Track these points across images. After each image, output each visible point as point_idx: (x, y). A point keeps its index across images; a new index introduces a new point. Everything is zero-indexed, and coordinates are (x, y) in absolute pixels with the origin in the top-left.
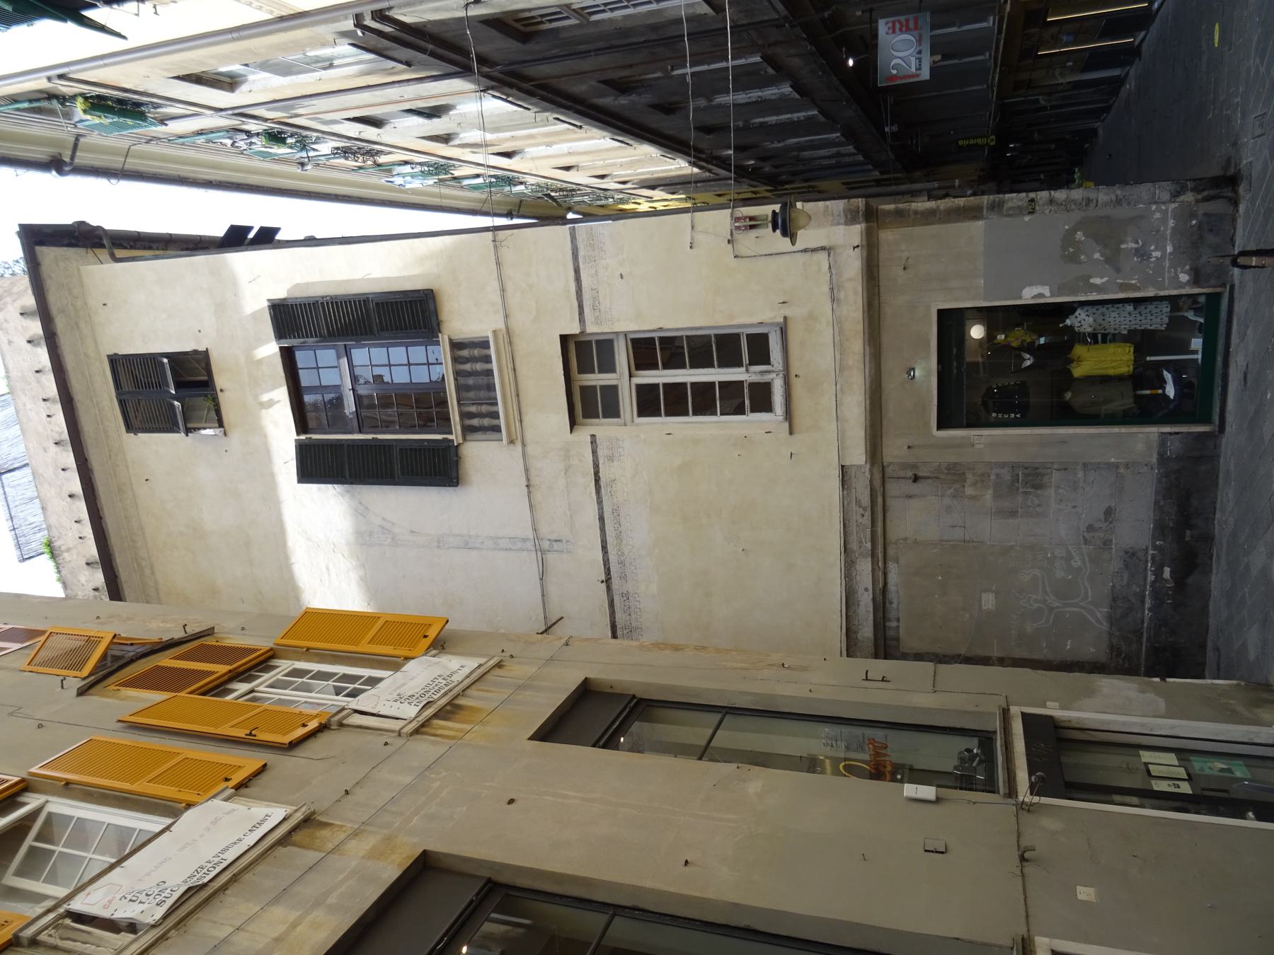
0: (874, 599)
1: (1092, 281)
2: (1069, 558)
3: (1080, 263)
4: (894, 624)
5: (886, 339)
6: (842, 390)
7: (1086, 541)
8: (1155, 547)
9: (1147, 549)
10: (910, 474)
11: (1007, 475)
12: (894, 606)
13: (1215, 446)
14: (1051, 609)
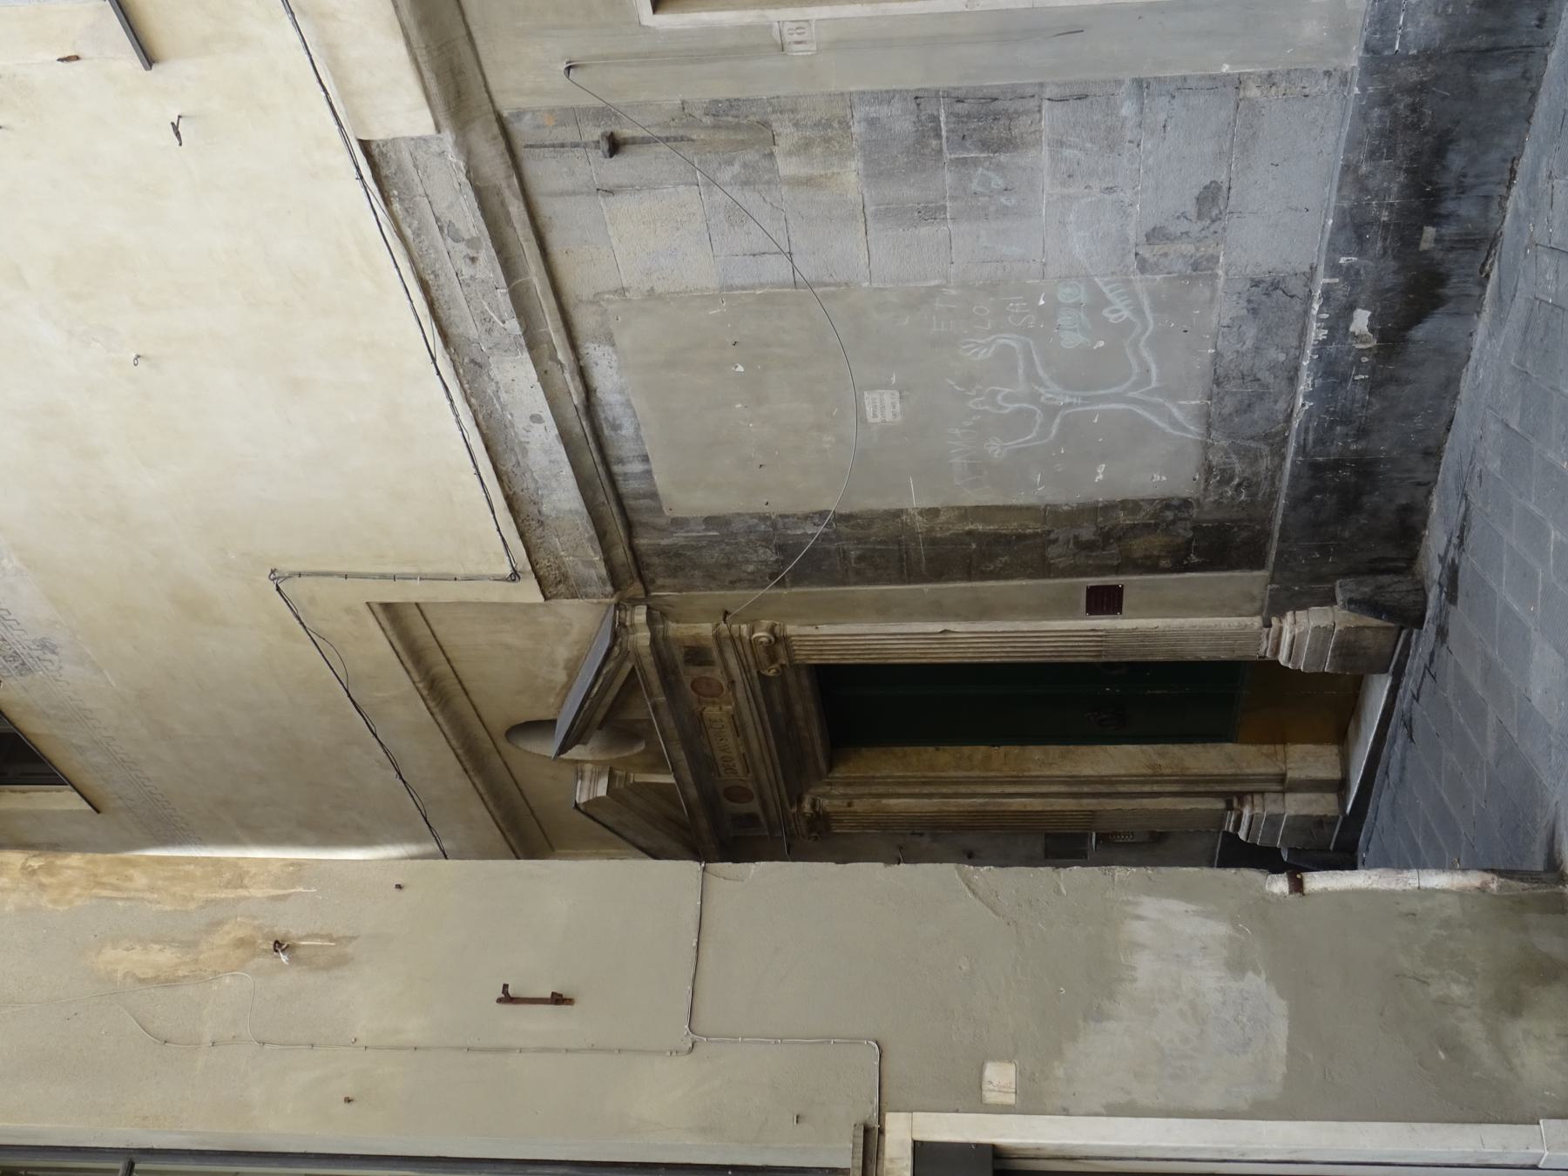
0: (565, 437)
2: (1098, 302)
4: (637, 467)
7: (1143, 266)
8: (1334, 269)
9: (1313, 269)
10: (594, 133)
11: (902, 123)
12: (627, 430)
13: (1541, 20)
14: (1051, 411)
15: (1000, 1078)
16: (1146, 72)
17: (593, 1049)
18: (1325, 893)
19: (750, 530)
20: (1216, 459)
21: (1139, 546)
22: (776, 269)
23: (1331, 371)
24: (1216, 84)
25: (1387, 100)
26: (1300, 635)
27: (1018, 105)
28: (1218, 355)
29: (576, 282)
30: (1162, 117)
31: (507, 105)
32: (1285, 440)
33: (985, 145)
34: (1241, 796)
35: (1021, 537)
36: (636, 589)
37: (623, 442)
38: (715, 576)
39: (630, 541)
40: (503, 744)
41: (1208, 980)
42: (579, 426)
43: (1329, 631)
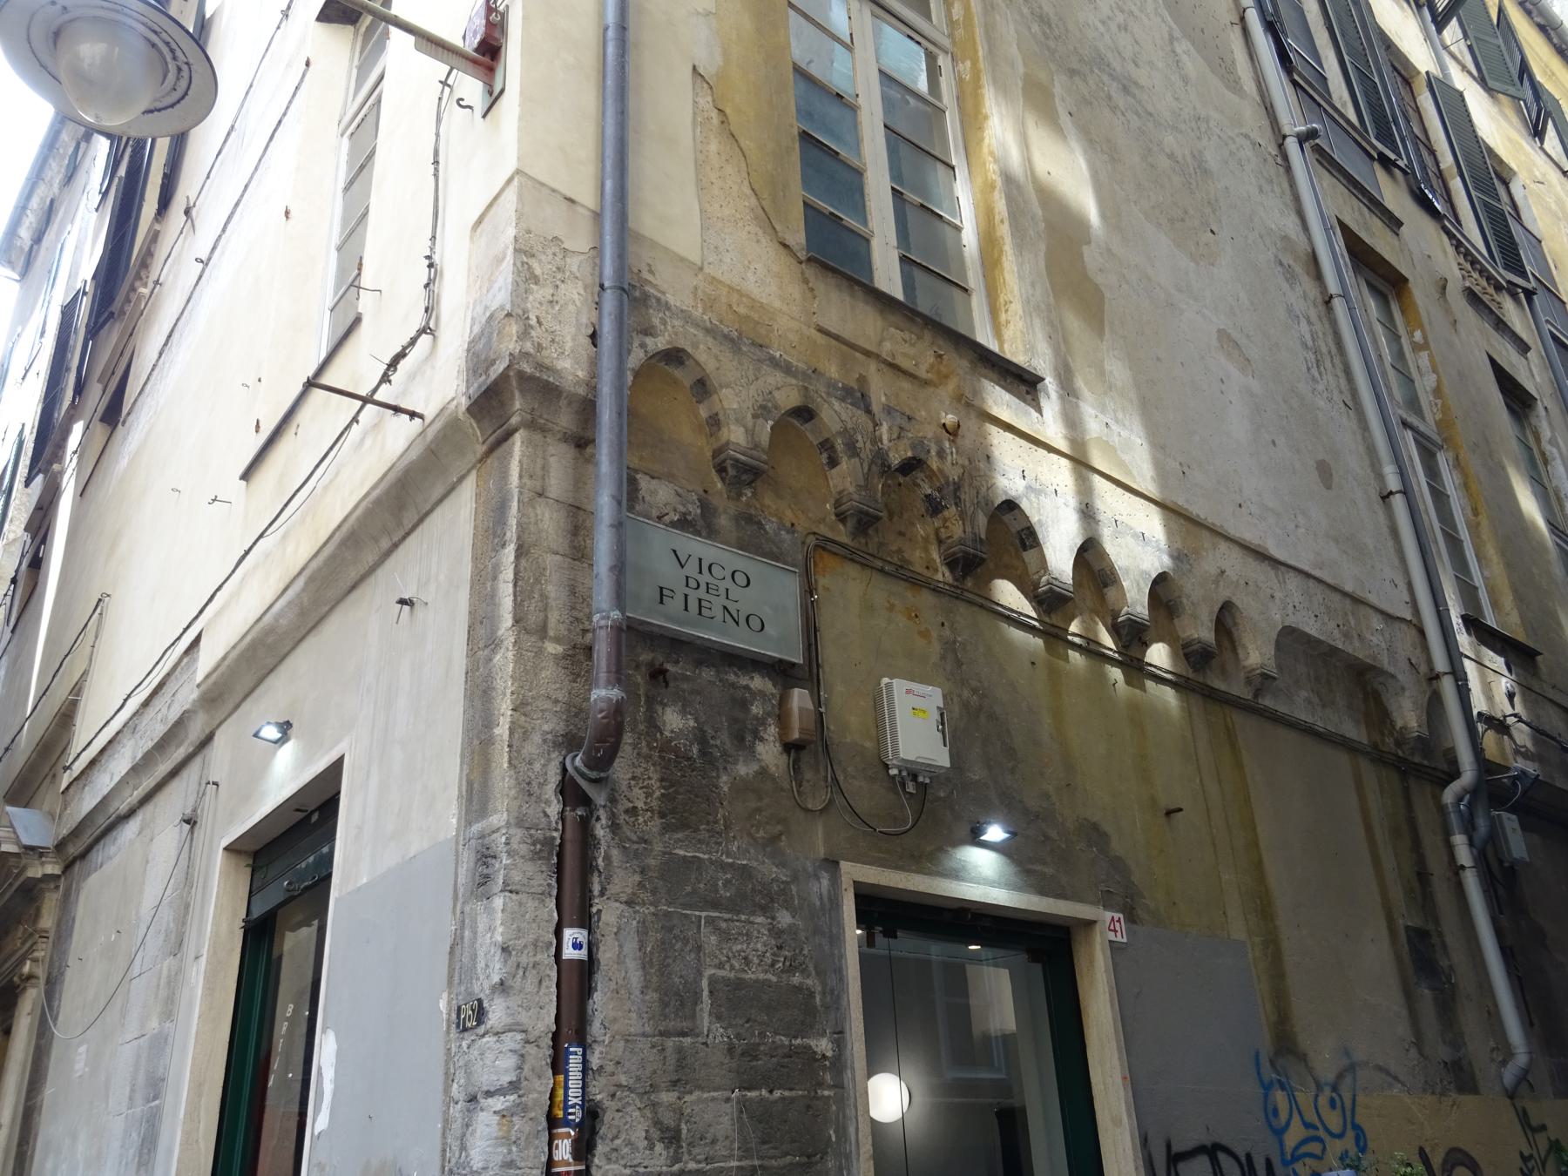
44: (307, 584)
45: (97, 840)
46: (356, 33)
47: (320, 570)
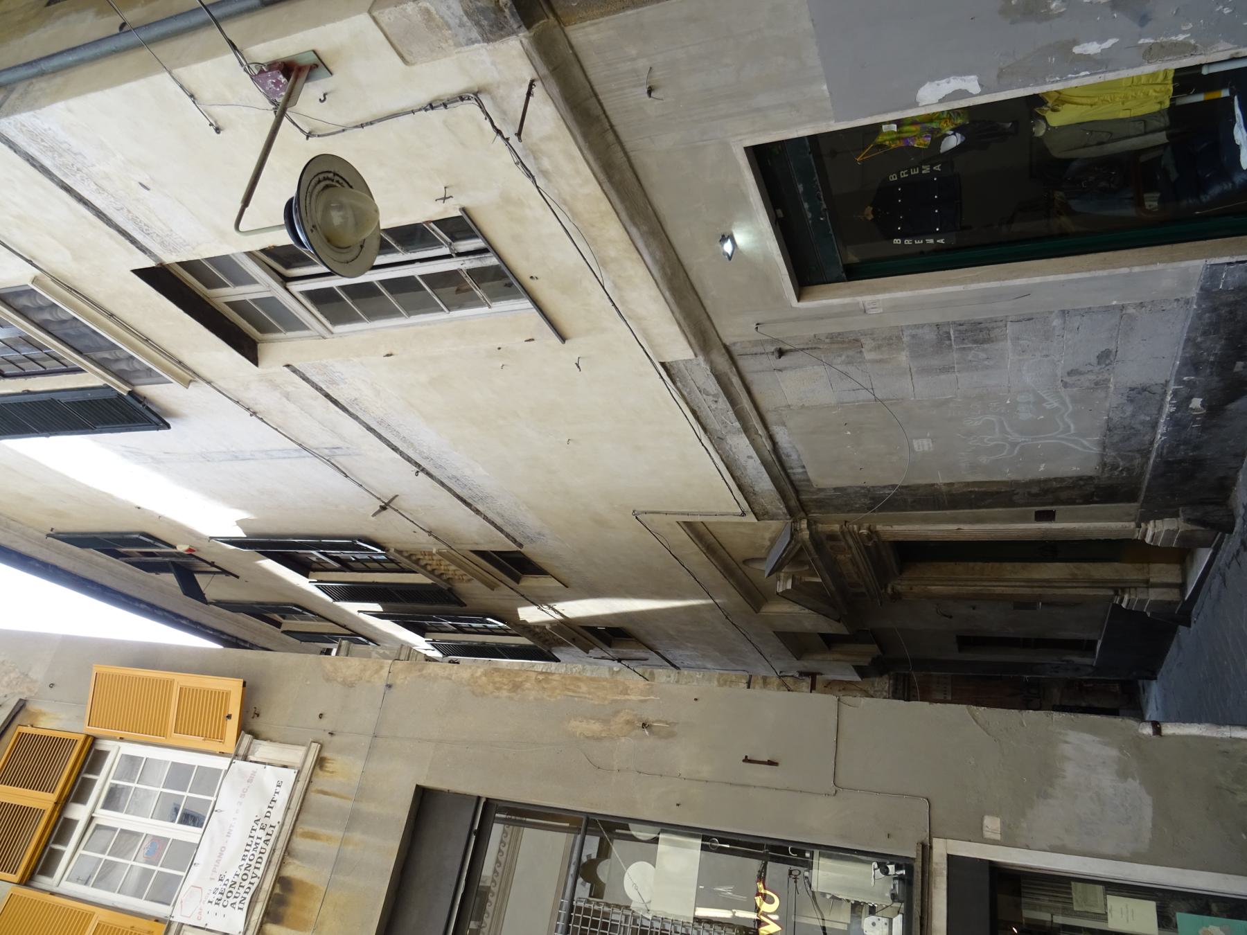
1: (1077, 50)
3: (1048, 16)
4: (800, 470)
5: (663, 201)
6: (616, 286)
7: (1065, 385)
8: (1179, 381)
9: (1167, 382)
11: (931, 336)
12: (794, 457)
14: (1014, 445)
15: (992, 825)
16: (1067, 307)
17: (788, 790)
18: (1174, 736)
19: (856, 492)
20: (1108, 460)
21: (1064, 495)
22: (864, 395)
23: (1176, 422)
24: (1108, 309)
25: (1214, 310)
26: (1156, 530)
27: (994, 325)
28: (1110, 419)
29: (764, 403)
30: (1076, 325)
31: (727, 341)
32: (1150, 452)
33: (975, 342)
34: (1123, 590)
35: (998, 493)
36: (802, 514)
37: (793, 460)
38: (838, 509)
39: (794, 492)
40: (742, 566)
41: (1107, 781)
42: (770, 457)
43: (1175, 532)
44: (635, 224)
45: (784, 468)
46: (262, 341)
47: (627, 209)
